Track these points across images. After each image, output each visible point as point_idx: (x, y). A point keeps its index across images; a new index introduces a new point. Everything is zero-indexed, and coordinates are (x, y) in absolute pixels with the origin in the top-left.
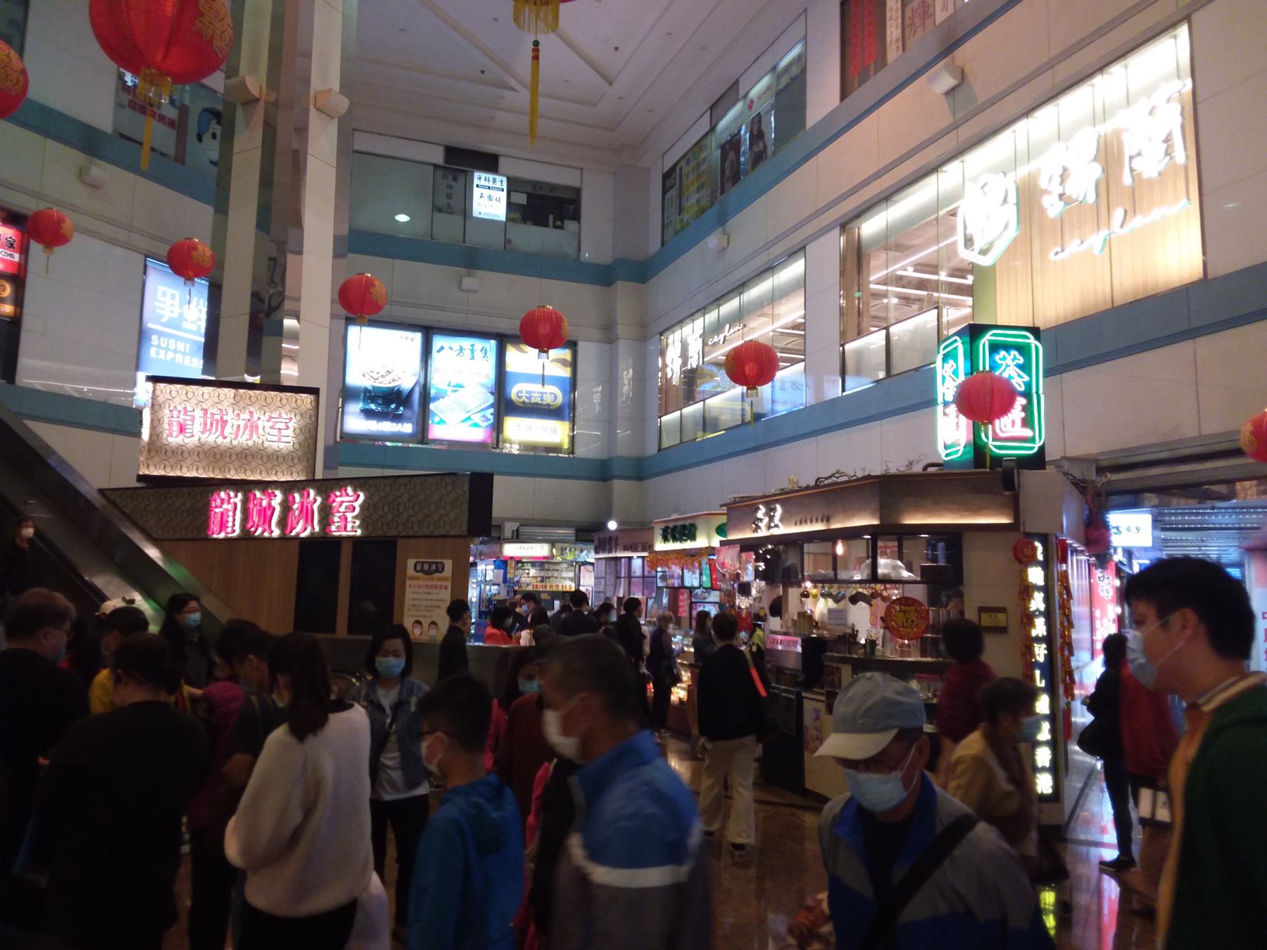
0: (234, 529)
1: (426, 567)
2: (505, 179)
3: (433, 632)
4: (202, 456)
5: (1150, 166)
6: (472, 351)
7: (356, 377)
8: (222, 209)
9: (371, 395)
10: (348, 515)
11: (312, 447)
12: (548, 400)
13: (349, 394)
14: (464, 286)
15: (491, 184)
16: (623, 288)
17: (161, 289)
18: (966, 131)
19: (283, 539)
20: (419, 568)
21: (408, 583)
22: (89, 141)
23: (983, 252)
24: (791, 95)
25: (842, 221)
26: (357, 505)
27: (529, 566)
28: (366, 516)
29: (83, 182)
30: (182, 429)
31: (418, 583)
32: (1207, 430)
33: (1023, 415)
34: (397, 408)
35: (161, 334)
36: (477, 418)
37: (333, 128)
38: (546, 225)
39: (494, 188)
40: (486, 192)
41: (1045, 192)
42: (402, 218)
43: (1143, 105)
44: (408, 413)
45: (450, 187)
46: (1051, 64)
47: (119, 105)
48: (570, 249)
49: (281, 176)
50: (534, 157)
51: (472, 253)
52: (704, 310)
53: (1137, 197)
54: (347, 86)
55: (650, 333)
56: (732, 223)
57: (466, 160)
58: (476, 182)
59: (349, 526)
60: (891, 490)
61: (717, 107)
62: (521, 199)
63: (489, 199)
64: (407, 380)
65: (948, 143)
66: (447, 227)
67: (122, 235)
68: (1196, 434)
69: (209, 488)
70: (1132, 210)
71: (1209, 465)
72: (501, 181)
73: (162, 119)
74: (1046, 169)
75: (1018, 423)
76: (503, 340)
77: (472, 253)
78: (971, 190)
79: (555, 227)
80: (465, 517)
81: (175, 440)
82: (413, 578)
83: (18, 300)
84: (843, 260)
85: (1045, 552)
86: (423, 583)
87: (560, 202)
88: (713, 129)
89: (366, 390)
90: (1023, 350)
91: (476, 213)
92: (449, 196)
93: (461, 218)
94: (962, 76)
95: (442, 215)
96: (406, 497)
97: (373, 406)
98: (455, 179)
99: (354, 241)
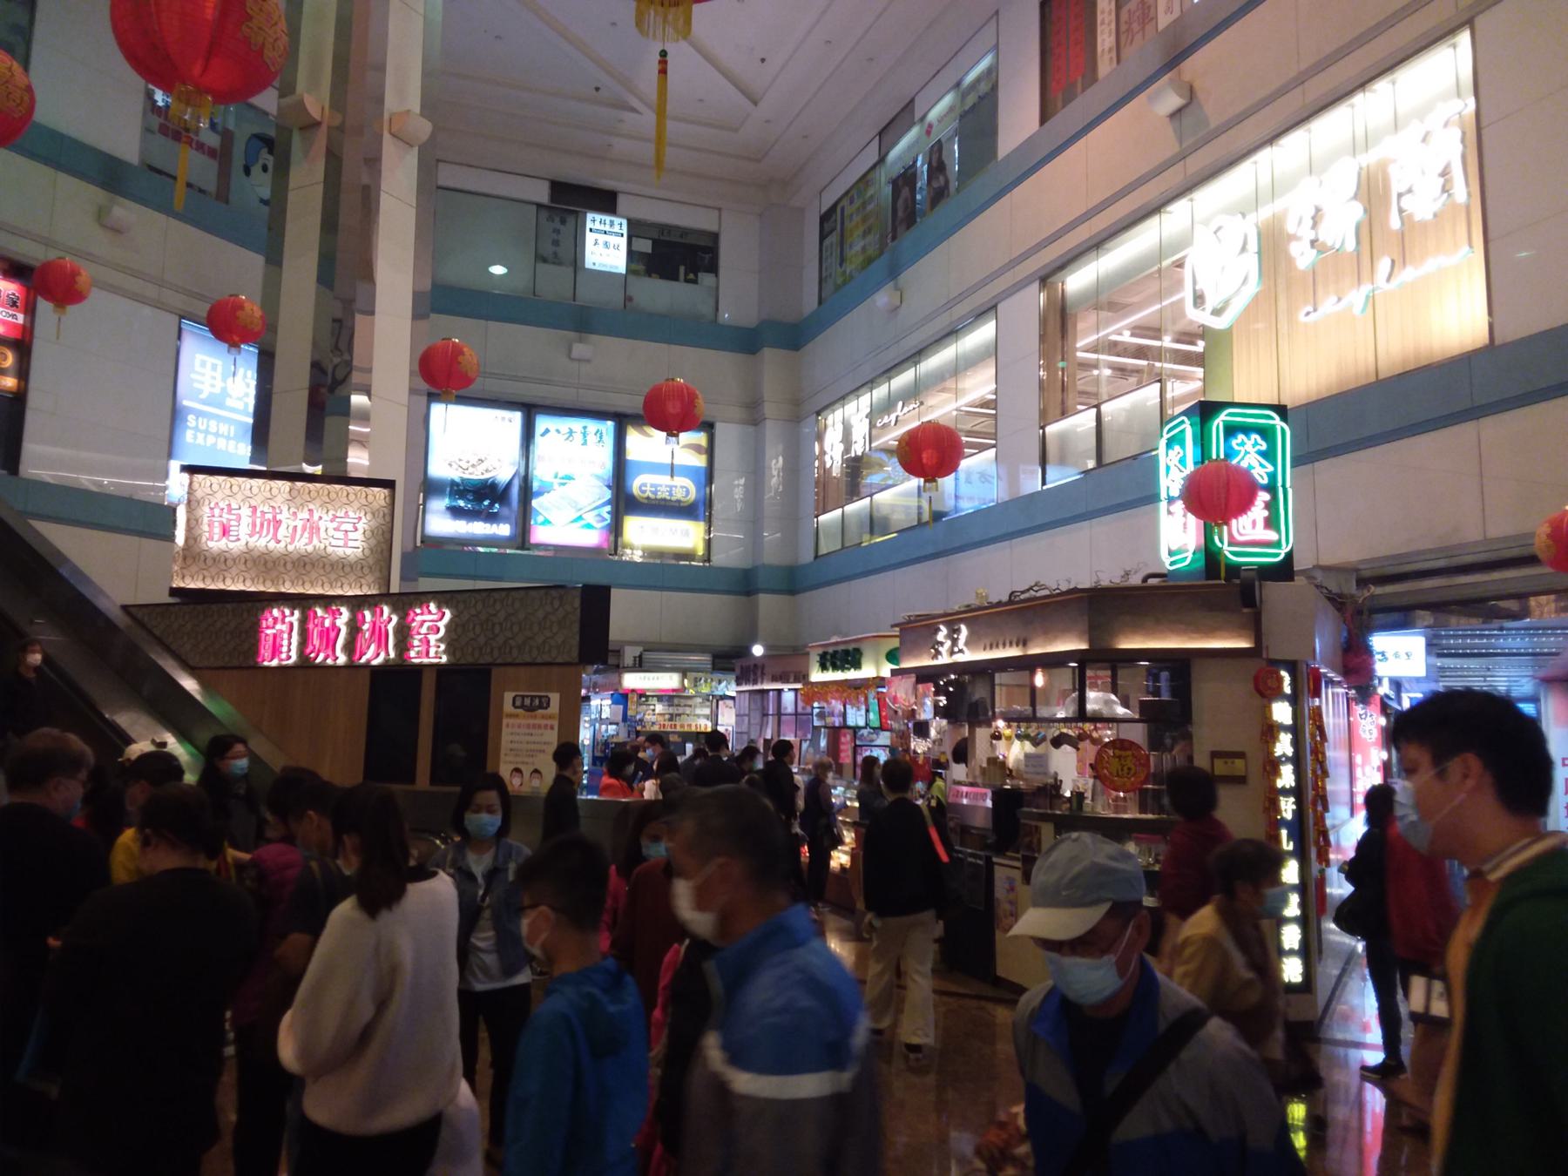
0: (290, 654)
1: (527, 702)
2: (625, 222)
3: (536, 783)
4: (249, 564)
5: (1424, 205)
6: (585, 435)
7: (440, 467)
8: (274, 258)
9: (459, 489)
10: (430, 637)
11: (386, 554)
12: (678, 495)
13: (431, 488)
14: (575, 354)
15: (607, 228)
16: (771, 357)
17: (199, 357)
18: (1196, 163)
19: (351, 667)
20: (518, 703)
21: (505, 721)
22: (110, 175)
23: (1217, 312)
24: (979, 118)
25: (1042, 273)
26: (442, 625)
27: (655, 701)
28: (454, 638)
29: (103, 226)
30: (225, 532)
31: (518, 721)
32: (1494, 532)
33: (1266, 513)
34: (491, 505)
35: (199, 414)
36: (591, 518)
37: (412, 159)
38: (675, 278)
39: (611, 233)
40: (602, 238)
41: (1293, 237)
42: (498, 270)
43: (1414, 130)
44: (505, 511)
45: (557, 231)
46: (1301, 80)
47: (147, 130)
48: (706, 309)
49: (348, 218)
50: (661, 194)
51: (584, 313)
52: (871, 383)
53: (1407, 243)
54: (429, 107)
55: (805, 412)
56: (906, 276)
57: (577, 199)
58: (589, 225)
59: (432, 651)
60: (1102, 606)
61: (888, 132)
62: (645, 246)
63: (605, 247)
64: (503, 470)
65: (1173, 178)
66: (553, 281)
67: (151, 291)
68: (1480, 538)
69: (258, 605)
70: (1401, 260)
71: (1496, 575)
72: (620, 225)
73: (200, 147)
74: (1294, 209)
75: (1260, 523)
76: (622, 421)
77: (584, 313)
78: (1202, 236)
79: (687, 281)
80: (575, 640)
81: (216, 544)
82: (511, 716)
83: (23, 372)
84: (1044, 322)
85: (1294, 684)
86: (523, 722)
87: (693, 250)
88: (882, 160)
89: (453, 483)
90: (1266, 433)
91: (589, 264)
92: (556, 243)
93: (571, 269)
94: (1191, 94)
95: (546, 266)
96: (502, 615)
97: (461, 503)
98: (563, 222)
99: (438, 299)
